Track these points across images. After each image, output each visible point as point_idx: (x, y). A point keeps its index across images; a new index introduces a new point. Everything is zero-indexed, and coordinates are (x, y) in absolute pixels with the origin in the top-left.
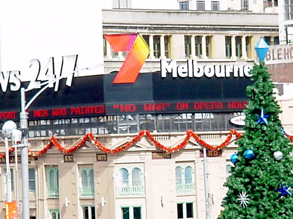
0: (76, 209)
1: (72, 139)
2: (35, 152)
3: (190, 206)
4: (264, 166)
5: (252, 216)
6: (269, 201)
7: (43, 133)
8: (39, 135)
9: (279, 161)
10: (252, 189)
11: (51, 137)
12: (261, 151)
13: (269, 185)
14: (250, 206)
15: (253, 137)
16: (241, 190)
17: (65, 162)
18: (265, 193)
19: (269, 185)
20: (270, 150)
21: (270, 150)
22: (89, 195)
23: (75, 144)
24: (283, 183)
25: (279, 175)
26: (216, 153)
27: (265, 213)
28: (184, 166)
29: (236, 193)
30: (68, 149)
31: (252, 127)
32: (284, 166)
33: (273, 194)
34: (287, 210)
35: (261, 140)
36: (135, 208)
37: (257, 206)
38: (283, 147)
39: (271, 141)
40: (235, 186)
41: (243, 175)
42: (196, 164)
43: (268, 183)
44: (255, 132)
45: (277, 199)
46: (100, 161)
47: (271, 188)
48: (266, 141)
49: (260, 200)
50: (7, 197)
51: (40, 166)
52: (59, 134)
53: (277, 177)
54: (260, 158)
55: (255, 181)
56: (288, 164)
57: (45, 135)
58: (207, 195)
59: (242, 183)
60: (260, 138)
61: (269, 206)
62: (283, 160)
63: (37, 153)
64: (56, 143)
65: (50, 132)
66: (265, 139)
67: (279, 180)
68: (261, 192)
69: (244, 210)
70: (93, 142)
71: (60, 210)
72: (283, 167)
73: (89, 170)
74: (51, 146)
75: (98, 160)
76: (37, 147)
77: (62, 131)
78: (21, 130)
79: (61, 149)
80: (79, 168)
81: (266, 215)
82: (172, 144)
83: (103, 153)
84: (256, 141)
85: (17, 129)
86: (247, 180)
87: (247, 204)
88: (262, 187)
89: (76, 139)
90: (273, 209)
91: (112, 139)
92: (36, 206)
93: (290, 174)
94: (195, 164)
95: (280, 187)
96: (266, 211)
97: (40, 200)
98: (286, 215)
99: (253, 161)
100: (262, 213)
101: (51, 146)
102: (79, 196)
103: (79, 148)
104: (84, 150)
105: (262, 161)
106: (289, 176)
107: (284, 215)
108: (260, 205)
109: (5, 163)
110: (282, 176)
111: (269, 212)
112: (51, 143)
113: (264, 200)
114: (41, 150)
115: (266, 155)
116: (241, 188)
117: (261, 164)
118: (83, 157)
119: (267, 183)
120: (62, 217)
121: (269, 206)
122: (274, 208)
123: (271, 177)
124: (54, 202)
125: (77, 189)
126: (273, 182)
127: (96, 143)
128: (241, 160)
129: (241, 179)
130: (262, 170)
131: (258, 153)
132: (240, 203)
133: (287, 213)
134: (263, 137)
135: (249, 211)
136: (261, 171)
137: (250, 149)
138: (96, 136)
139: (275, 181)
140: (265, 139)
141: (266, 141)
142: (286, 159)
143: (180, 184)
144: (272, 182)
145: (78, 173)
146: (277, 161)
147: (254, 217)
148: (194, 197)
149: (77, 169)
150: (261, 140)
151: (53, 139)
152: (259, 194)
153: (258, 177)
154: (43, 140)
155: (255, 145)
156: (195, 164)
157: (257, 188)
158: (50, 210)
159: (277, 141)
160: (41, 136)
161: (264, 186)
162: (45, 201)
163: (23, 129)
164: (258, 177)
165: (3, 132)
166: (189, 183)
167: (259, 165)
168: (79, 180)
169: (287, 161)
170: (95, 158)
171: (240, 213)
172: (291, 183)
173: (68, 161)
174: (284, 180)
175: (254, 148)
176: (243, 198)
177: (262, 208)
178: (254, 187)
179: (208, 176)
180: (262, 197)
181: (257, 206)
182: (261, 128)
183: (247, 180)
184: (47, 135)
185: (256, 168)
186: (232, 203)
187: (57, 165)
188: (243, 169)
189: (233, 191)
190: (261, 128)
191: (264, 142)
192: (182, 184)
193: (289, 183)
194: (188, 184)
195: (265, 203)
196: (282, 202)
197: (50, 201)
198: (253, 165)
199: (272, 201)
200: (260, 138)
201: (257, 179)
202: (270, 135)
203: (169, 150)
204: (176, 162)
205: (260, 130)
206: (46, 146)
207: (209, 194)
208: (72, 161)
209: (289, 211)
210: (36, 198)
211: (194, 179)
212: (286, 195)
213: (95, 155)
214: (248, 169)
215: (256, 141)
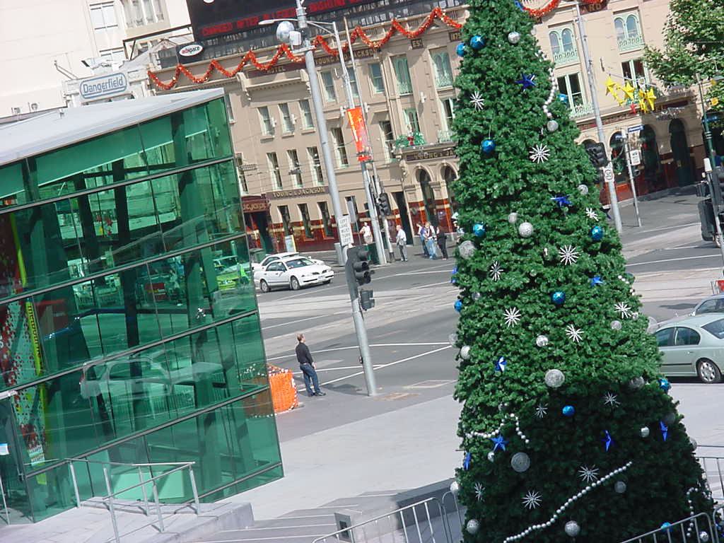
0: (435, 104)
1: (416, 19)
2: (376, 42)
3: (574, 79)
4: (498, 54)
5: (489, 120)
6: (509, 98)
7: (383, 16)
8: (379, 20)
9: (516, 45)
10: (486, 85)
11: (392, 20)
12: (492, 36)
13: (505, 78)
14: (486, 108)
15: (480, 18)
16: (473, 90)
18: (502, 90)
19: (505, 78)
20: (503, 33)
21: (503, 33)
22: (448, 85)
23: (422, 25)
24: (525, 71)
25: (517, 62)
26: (599, 6)
27: (506, 114)
28: (559, 30)
29: (467, 94)
30: (414, 32)
31: (476, 5)
32: (523, 49)
33: (513, 88)
34: (533, 106)
35: (489, 21)
36: (570, 76)
37: (495, 107)
38: (519, 24)
39: (503, 20)
40: (465, 86)
41: (473, 70)
42: (641, 11)
43: (505, 75)
44: (482, 12)
45: (519, 93)
46: (454, 41)
47: (510, 81)
48: (496, 21)
49: (497, 98)
50: (348, 103)
51: (385, 58)
52: (403, 16)
53: (515, 65)
54: (491, 44)
55: (488, 76)
56: (528, 46)
57: (385, 19)
58: (588, 63)
59: (472, 81)
60: (489, 18)
61: (509, 104)
62: (522, 42)
63: (378, 43)
64: (399, 27)
65: (391, 15)
66: (494, 18)
67: (519, 69)
68: (497, 88)
69: (479, 114)
70: (442, 19)
71: (417, 108)
72: (522, 51)
73: (443, 54)
74: (394, 31)
75: (452, 41)
76: (378, 35)
77: (405, 11)
78: (300, 31)
79: (406, 34)
80: (431, 54)
81: (507, 116)
82: (541, 4)
83: (456, 30)
84: (484, 24)
85: (295, 30)
86: (478, 76)
87: (483, 106)
88: (497, 81)
89: (422, 18)
90: (514, 108)
91: (464, 12)
92: (388, 108)
93: (532, 58)
94: (639, 11)
95: (521, 78)
96: (507, 111)
97: (392, 100)
98: (534, 112)
99: (482, 50)
100: (501, 114)
101: (394, 31)
102: (436, 87)
103: (427, 28)
104: (433, 30)
105: (494, 48)
106: (531, 61)
107: (531, 112)
108: (499, 105)
109: (340, 61)
110: (523, 63)
111: (510, 112)
112: (393, 28)
113: (502, 98)
114: (382, 38)
115: (499, 40)
116: (472, 87)
117: (493, 52)
118: (435, 39)
119: (502, 75)
120: (420, 116)
121: (509, 104)
122: (516, 106)
123: (508, 67)
124: (408, 99)
125: (432, 80)
126: (511, 73)
127: (445, 19)
128: (468, 51)
129: (471, 75)
130: (496, 60)
131: (488, 39)
132: (474, 107)
133: (534, 109)
134: (492, 16)
135: (485, 115)
136: (494, 61)
137: (478, 35)
138: (445, 10)
139: (512, 72)
140: (494, 18)
141: (496, 21)
142: (526, 40)
143: (558, 53)
144: (509, 73)
145: (431, 61)
146: (513, 44)
147: (492, 122)
148: (579, 65)
149: (429, 55)
150: (489, 21)
151: (394, 22)
152: (495, 92)
153: (491, 69)
154: (384, 26)
155: (482, 28)
156: (639, 11)
157: (492, 84)
158: (405, 111)
159: (511, 18)
160: (381, 21)
161: (500, 80)
162: (397, 100)
163: (303, 29)
164: (491, 69)
165: (278, 37)
166: (570, 50)
167: (491, 54)
168: (434, 68)
169: (527, 42)
170: (448, 38)
171: (476, 119)
172: (535, 70)
173: (417, 48)
174: (525, 68)
175: (482, 33)
176: (477, 99)
177: (502, 109)
178: (488, 83)
179: (586, 38)
180: (499, 94)
181: (495, 107)
182: (488, 6)
183: (478, 76)
184: (388, 19)
185: (487, 58)
186: (465, 108)
187: (405, 54)
188: (472, 63)
189: (463, 93)
190: (488, 6)
191: (494, 23)
192: (560, 53)
193: (533, 70)
194: (568, 51)
195: (505, 102)
196: (525, 96)
197: (403, 99)
198: (482, 56)
199: (512, 98)
200: (489, 18)
201: (491, 72)
202: (500, 13)
203: (538, 12)
204: (549, 27)
205: (487, 8)
206: (388, 33)
207: (590, 61)
209: (537, 106)
210: (386, 99)
211: (640, 29)
212: (530, 87)
214: (477, 62)
215: (484, 24)
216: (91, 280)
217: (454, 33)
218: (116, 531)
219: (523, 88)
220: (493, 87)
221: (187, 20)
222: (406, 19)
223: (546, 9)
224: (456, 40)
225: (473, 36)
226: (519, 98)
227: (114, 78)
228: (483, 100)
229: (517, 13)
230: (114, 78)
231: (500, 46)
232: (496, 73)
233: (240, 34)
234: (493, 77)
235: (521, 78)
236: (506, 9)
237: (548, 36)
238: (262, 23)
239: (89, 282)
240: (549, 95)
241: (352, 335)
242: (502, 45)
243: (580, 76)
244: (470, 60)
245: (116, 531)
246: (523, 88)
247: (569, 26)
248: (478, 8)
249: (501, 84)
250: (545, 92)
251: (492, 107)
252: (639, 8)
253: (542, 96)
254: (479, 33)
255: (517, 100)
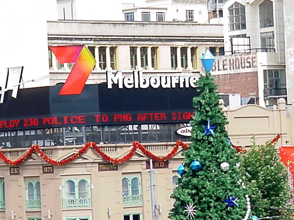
1: (18, 151)
4: (211, 177)
6: (216, 212)
9: (226, 172)
13: (215, 196)
15: (200, 148)
16: (189, 202)
17: (11, 174)
18: (212, 205)
20: (217, 161)
21: (217, 161)
23: (21, 156)
25: (226, 186)
26: (162, 164)
28: (130, 178)
29: (183, 204)
31: (199, 138)
32: (231, 177)
35: (207, 151)
38: (229, 158)
39: (217, 152)
43: (215, 194)
44: (202, 144)
45: (224, 210)
47: (218, 199)
48: (212, 152)
53: (224, 188)
54: (207, 169)
55: (202, 193)
56: (234, 175)
58: (154, 206)
60: (207, 149)
61: (216, 217)
62: (230, 171)
66: (212, 150)
67: (226, 191)
72: (229, 178)
75: (44, 173)
84: (203, 153)
86: (194, 191)
87: (194, 215)
89: (22, 151)
95: (227, 198)
105: (208, 172)
106: (235, 187)
110: (229, 187)
113: (211, 211)
115: (213, 167)
119: (214, 194)
126: (220, 193)
128: (188, 171)
129: (188, 190)
130: (209, 181)
132: (187, 215)
134: (210, 148)
136: (208, 182)
140: (212, 150)
141: (212, 152)
142: (233, 170)
143: (127, 195)
144: (219, 193)
150: (207, 151)
152: (206, 206)
153: (205, 188)
156: (141, 175)
157: (204, 199)
161: (211, 197)
164: (205, 188)
166: (136, 194)
167: (206, 176)
170: (42, 170)
174: (231, 191)
175: (201, 159)
176: (190, 209)
179: (155, 187)
180: (209, 208)
182: (208, 140)
183: (194, 191)
185: (203, 179)
188: (190, 181)
190: (208, 140)
191: (210, 153)
192: (128, 196)
193: (236, 194)
194: (135, 195)
199: (219, 212)
207: (155, 205)
208: (18, 174)
212: (233, 206)
213: (41, 167)
214: (195, 181)
215: (203, 153)
217: (47, 166)
219: (227, 207)
220: (205, 201)
222: (9, 150)
223: (122, 159)
224: (47, 173)
225: (193, 161)
226: (224, 213)
228: (196, 210)
229: (229, 148)
231: (213, 171)
232: (209, 192)
234: (206, 193)
235: (227, 198)
236: (221, 144)
237: (172, 178)
240: (245, 215)
242: (215, 171)
243: (141, 216)
244: (189, 178)
246: (227, 207)
247: (138, 176)
248: (199, 141)
249: (212, 200)
250: (243, 212)
251: (202, 217)
252: (142, 173)
253: (241, 215)
254: (199, 159)
255: (222, 215)
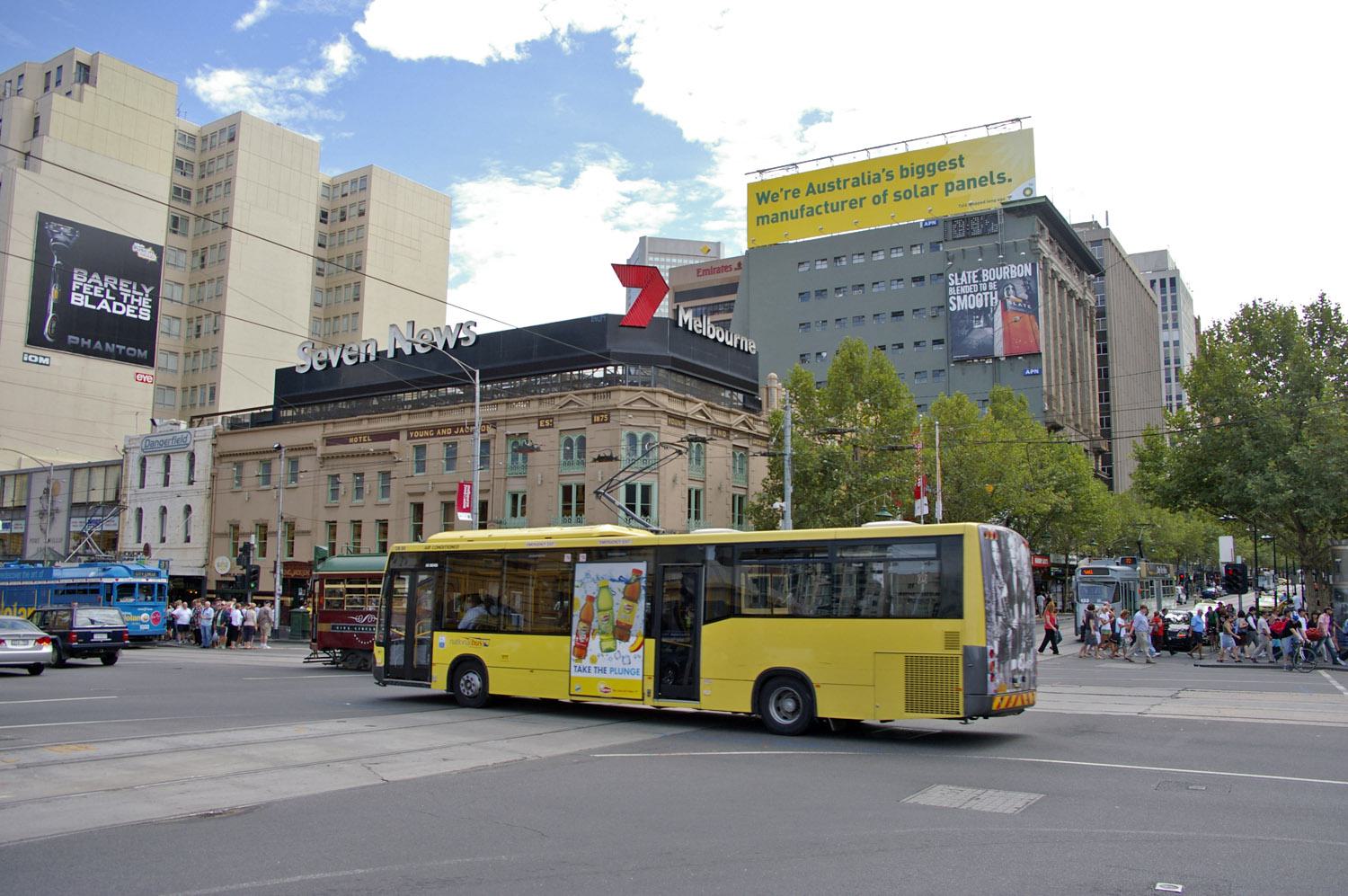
36: (1171, 279)
216: (813, 558)
218: (88, 494)
221: (871, 157)
227: (179, 436)
230: (179, 436)
233: (297, 410)
238: (427, 565)
239: (816, 555)
241: (74, 513)
245: (88, 494)
